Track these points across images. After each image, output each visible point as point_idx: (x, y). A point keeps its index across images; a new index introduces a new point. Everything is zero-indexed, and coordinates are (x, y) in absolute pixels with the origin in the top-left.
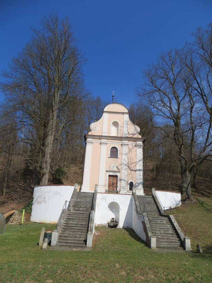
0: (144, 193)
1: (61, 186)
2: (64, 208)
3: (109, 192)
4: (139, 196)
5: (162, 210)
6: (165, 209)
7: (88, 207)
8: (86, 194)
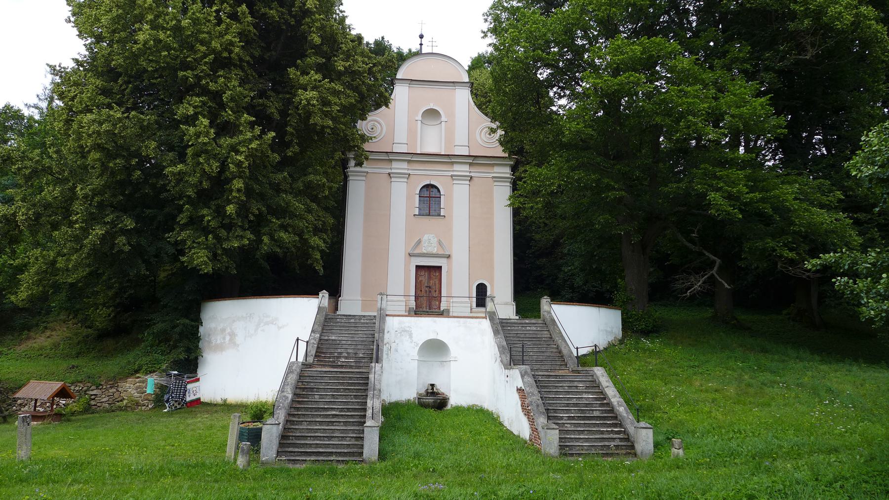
0: (518, 313)
1: (279, 300)
2: (293, 359)
3: (418, 312)
4: (504, 321)
5: (570, 357)
6: (582, 352)
7: (361, 355)
8: (352, 321)
